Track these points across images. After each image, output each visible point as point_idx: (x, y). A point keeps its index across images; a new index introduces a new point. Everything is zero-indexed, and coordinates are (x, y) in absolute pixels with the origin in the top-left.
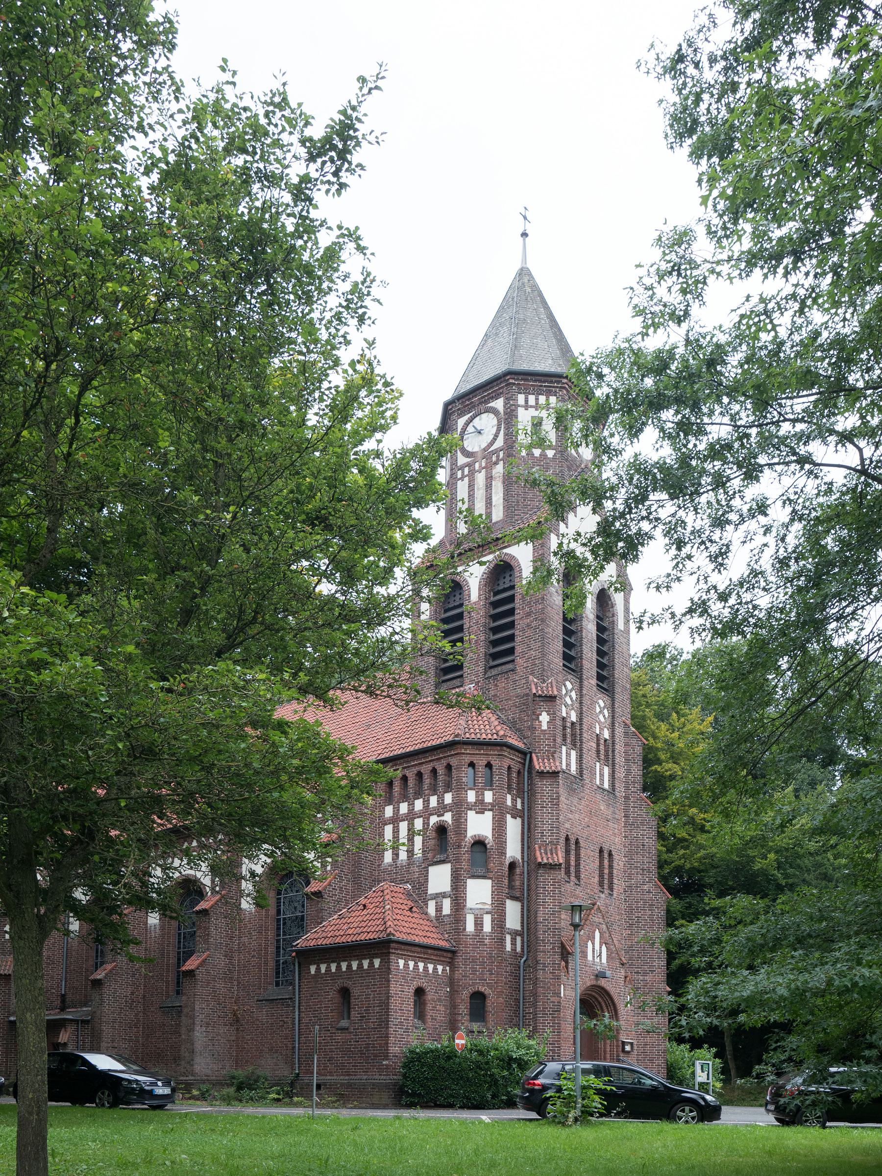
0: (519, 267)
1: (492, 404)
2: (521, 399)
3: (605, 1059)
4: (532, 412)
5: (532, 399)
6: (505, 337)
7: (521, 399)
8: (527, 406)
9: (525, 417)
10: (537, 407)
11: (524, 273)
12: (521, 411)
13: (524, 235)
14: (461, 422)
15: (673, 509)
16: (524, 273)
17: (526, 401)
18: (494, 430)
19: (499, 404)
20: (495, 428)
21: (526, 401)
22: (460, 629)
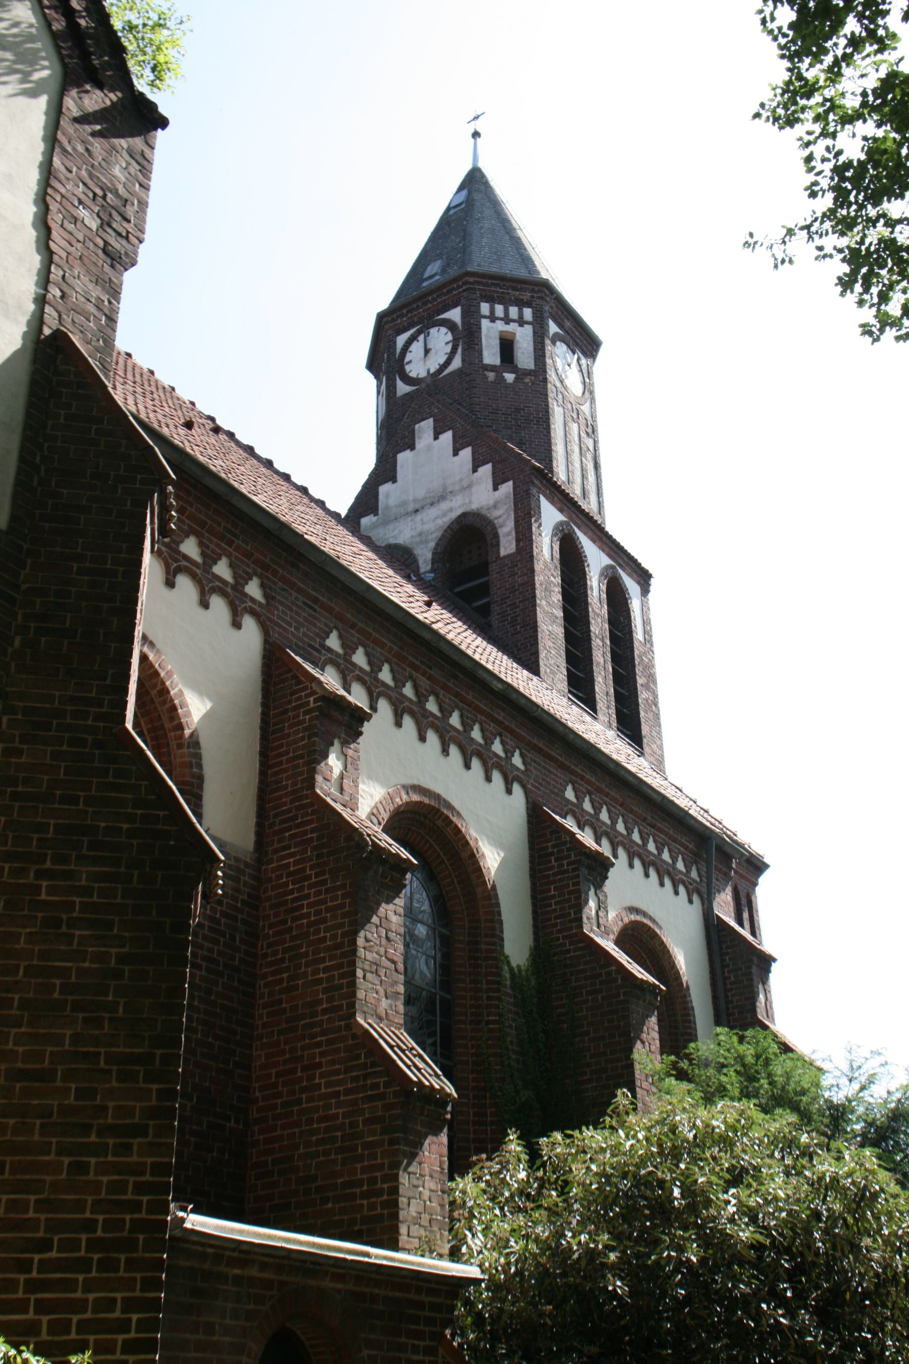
0: (469, 167)
1: (446, 315)
2: (485, 308)
3: (118, 1047)
4: (500, 326)
5: (499, 310)
6: (464, 193)
7: (485, 308)
8: (493, 318)
9: (490, 333)
10: (507, 320)
11: (475, 182)
12: (485, 323)
13: (476, 135)
14: (401, 340)
15: (749, 1177)
16: (475, 182)
17: (492, 311)
18: (448, 349)
19: (455, 314)
20: (450, 346)
21: (492, 311)
22: (484, 590)
